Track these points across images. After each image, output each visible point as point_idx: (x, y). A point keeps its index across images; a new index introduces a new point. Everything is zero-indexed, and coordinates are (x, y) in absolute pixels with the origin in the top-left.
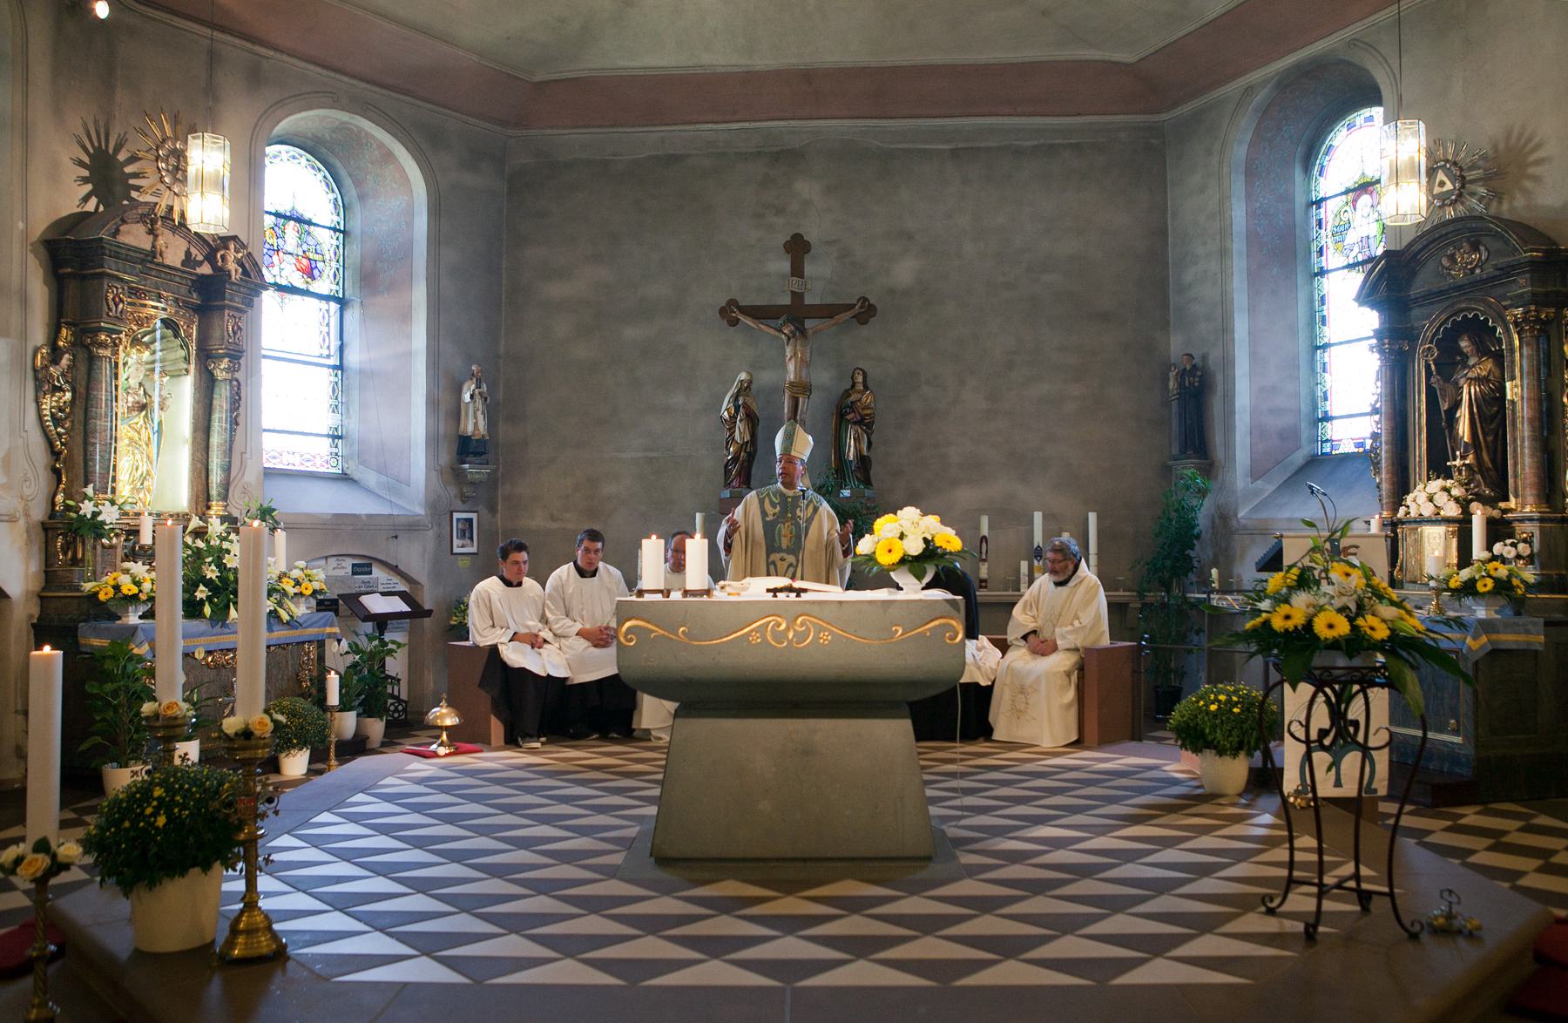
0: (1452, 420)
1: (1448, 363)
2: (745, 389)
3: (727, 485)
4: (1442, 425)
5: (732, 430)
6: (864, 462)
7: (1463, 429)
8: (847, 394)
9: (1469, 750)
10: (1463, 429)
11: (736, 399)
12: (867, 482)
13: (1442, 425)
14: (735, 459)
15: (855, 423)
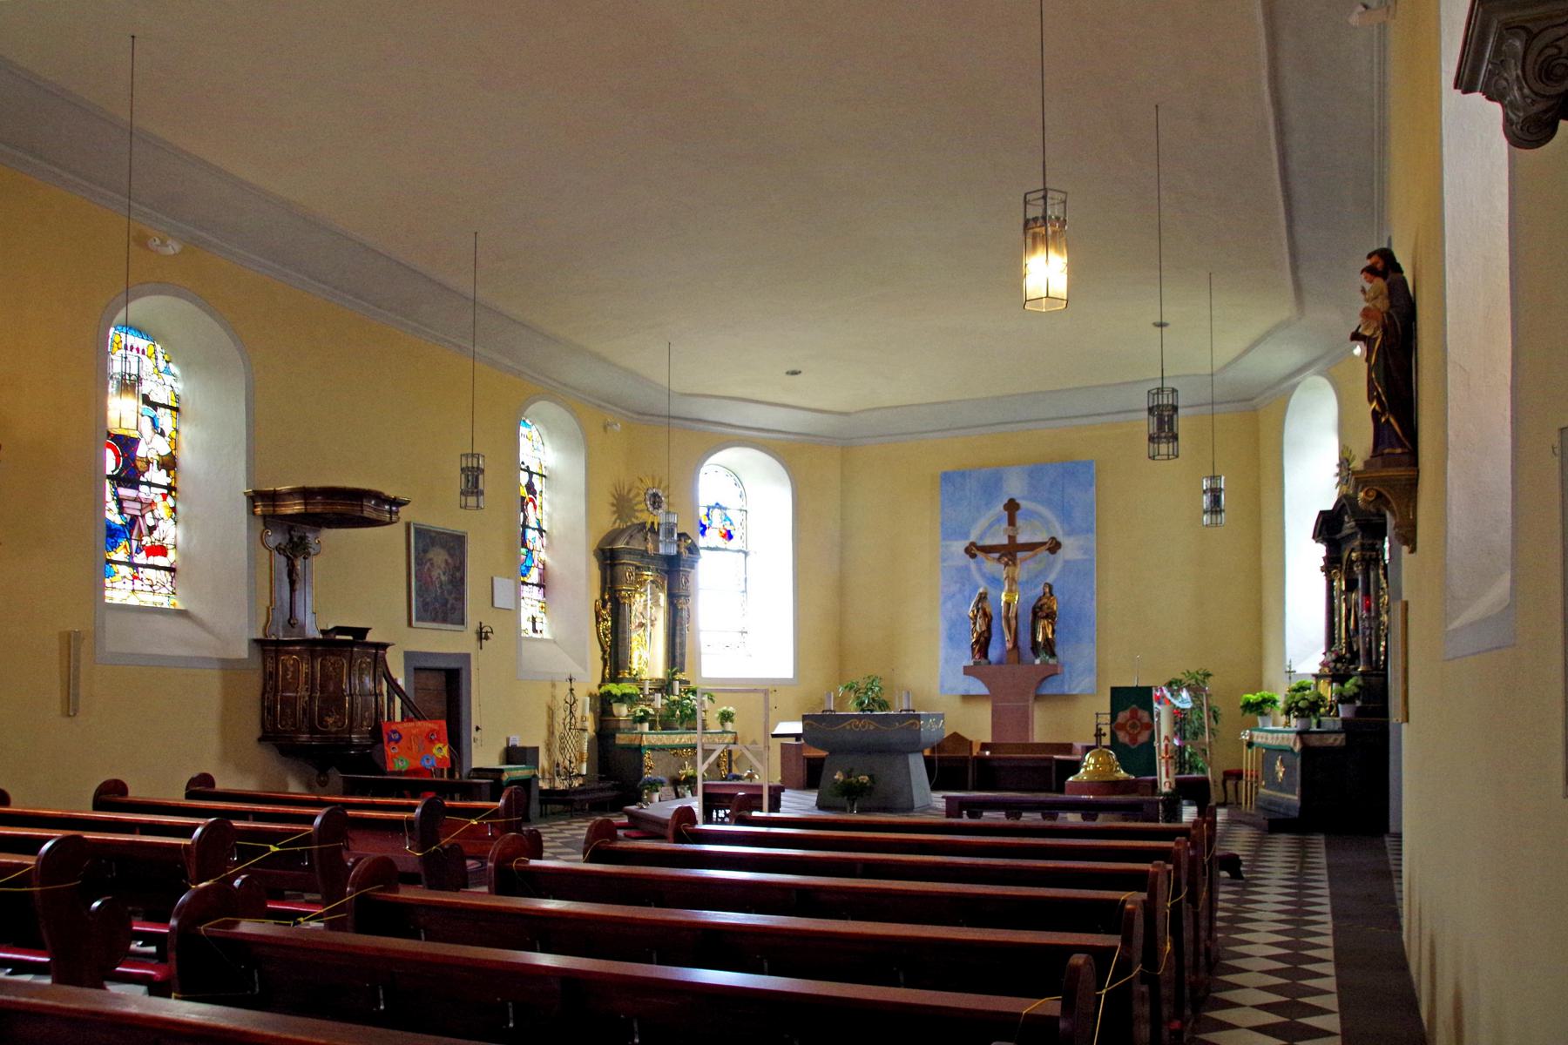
9: (1299, 804)
12: (1053, 655)
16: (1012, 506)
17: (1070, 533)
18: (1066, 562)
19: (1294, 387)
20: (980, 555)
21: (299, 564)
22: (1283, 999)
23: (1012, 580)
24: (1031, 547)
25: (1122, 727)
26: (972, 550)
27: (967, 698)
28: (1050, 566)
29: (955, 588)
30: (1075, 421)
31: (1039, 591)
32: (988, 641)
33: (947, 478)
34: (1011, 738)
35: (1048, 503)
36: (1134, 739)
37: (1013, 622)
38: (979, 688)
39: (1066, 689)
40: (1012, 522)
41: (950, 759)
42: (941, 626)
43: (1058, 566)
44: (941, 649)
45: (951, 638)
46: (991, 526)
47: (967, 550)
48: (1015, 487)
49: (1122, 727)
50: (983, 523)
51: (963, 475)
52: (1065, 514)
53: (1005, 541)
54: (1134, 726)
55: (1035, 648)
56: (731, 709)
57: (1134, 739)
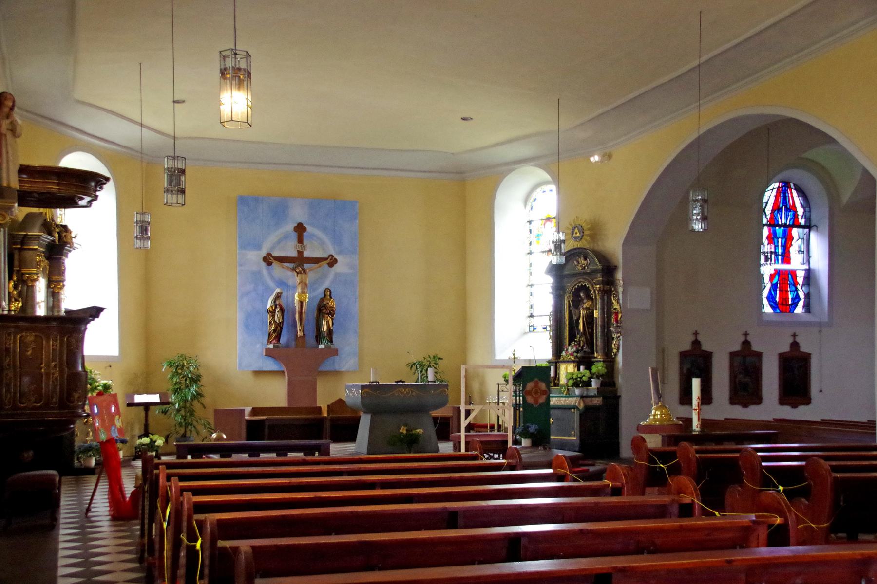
0: (578, 323)
1: (576, 303)
2: (278, 296)
3: (269, 342)
4: (573, 326)
5: (273, 317)
6: (330, 332)
7: (581, 327)
8: (322, 300)
9: (578, 442)
10: (581, 327)
11: (275, 302)
12: (331, 341)
13: (573, 326)
14: (275, 331)
15: (328, 314)
16: (300, 229)
17: (340, 252)
18: (337, 275)
19: (510, 171)
20: (275, 264)
21: (291, 265)
22: (82, 579)
23: (304, 285)
24: (316, 261)
25: (529, 393)
26: (268, 260)
27: (258, 373)
28: (325, 276)
29: (249, 287)
30: (393, 173)
31: (319, 293)
32: (281, 328)
33: (243, 201)
34: (303, 403)
35: (324, 229)
36: (536, 401)
37: (304, 316)
38: (271, 365)
39: (337, 369)
40: (300, 240)
41: (339, 419)
42: (239, 317)
43: (331, 277)
44: (239, 335)
45: (247, 326)
46: (279, 242)
47: (265, 259)
48: (298, 214)
49: (529, 393)
50: (273, 238)
51: (257, 199)
52: (337, 239)
53: (294, 254)
54: (536, 392)
55: (319, 338)
56: (110, 383)
57: (536, 401)
